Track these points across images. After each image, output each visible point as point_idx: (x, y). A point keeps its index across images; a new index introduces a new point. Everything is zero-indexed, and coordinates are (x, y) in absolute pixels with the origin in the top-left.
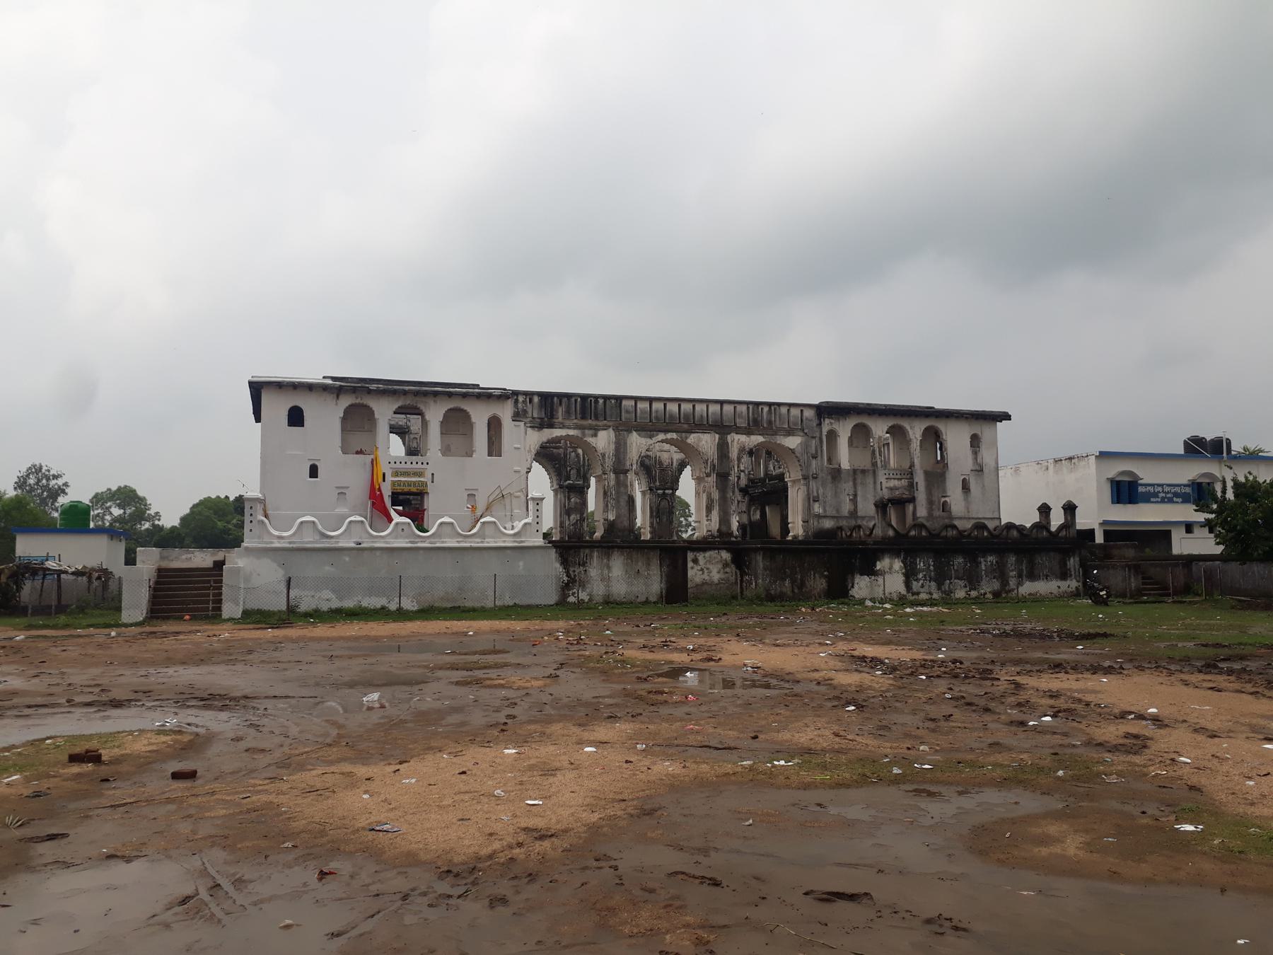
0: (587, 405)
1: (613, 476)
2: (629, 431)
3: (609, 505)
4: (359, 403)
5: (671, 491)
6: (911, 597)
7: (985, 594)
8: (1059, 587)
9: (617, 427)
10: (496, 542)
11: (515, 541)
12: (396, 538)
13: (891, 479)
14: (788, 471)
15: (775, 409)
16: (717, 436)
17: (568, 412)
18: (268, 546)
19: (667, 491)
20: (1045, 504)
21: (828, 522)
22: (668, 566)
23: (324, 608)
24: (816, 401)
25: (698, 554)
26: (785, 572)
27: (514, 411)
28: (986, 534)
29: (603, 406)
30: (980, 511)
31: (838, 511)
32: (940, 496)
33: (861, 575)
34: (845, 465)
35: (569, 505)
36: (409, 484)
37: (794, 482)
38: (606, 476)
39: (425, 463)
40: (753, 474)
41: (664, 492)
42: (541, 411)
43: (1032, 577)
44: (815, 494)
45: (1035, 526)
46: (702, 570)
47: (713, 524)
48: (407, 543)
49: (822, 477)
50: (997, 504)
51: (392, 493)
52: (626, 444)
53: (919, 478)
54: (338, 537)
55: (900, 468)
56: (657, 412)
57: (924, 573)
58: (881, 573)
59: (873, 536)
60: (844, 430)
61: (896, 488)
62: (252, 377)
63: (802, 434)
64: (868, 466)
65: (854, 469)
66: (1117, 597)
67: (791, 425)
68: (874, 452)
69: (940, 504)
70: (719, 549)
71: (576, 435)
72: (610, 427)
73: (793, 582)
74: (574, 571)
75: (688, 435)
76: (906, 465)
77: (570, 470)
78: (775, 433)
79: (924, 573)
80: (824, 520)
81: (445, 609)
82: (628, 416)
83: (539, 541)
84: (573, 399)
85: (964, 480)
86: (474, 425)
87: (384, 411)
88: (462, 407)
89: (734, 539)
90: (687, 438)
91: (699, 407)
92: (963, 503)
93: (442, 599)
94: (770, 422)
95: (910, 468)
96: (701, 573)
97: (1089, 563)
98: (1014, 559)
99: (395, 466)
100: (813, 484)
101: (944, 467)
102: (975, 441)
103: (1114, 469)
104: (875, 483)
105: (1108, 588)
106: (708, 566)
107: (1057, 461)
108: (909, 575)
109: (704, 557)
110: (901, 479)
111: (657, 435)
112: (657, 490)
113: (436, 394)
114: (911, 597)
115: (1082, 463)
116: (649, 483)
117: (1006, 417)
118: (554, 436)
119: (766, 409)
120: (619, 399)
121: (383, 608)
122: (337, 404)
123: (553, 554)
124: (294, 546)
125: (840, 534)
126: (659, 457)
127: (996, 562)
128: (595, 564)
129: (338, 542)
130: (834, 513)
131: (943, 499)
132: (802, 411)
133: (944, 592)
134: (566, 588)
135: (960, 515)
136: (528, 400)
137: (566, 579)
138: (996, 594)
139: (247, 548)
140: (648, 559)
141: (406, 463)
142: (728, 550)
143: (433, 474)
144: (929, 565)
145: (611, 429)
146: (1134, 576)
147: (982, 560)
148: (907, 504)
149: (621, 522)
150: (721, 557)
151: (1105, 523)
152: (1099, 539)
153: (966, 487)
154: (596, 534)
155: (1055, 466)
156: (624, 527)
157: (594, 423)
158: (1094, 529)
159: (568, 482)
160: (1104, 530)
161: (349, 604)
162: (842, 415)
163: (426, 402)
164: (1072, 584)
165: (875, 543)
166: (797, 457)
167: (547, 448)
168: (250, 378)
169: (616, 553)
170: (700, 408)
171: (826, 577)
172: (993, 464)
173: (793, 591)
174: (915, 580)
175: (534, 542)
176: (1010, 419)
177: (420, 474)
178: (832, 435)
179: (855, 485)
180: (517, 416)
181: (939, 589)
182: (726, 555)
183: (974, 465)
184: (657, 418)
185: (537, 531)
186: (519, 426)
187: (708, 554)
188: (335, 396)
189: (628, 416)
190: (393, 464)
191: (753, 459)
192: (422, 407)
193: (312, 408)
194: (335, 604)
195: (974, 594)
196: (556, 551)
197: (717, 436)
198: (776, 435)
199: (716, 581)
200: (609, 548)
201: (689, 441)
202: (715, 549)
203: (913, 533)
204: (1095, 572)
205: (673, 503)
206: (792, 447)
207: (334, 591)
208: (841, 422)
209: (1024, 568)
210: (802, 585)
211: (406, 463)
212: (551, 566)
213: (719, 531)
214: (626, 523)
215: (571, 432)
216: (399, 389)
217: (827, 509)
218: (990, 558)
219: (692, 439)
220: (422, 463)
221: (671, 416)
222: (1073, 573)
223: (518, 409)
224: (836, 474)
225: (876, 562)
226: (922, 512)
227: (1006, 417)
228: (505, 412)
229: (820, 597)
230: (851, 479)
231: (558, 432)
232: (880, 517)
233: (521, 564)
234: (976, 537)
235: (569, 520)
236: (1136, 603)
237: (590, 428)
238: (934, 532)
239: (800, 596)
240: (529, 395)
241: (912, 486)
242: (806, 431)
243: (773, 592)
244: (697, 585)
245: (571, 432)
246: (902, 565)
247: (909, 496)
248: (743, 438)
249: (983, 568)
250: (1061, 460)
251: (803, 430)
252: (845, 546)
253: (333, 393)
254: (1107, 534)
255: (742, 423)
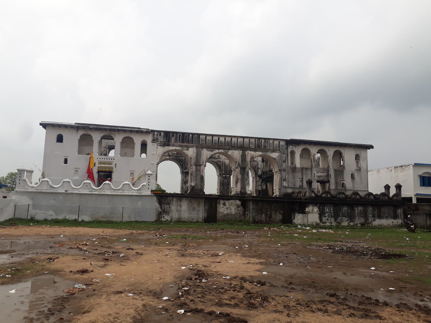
0: (184, 137)
1: (194, 167)
2: (203, 148)
3: (192, 179)
4: (87, 134)
5: (229, 176)
6: (322, 224)
7: (357, 224)
8: (393, 222)
9: (197, 146)
10: (129, 193)
11: (137, 193)
12: (84, 189)
13: (319, 172)
14: (274, 168)
15: (267, 141)
16: (241, 152)
17: (176, 140)
18: (26, 190)
19: (227, 176)
20: (388, 184)
21: (289, 190)
22: (208, 206)
23: (49, 218)
24: (288, 138)
25: (226, 201)
26: (263, 211)
27: (153, 139)
28: (358, 197)
29: (191, 138)
30: (359, 187)
31: (294, 185)
32: (341, 180)
33: (299, 213)
34: (298, 165)
35: (185, 180)
36: (105, 168)
37: (276, 172)
38: (192, 167)
39: (113, 159)
40: (264, 170)
41: (226, 176)
42: (164, 139)
43: (380, 217)
44: (284, 178)
45: (382, 194)
46: (227, 208)
47: (238, 189)
48: (88, 192)
49: (288, 170)
50: (367, 185)
51: (98, 171)
52: (201, 154)
53: (332, 172)
54: (58, 188)
55: (324, 168)
56: (215, 141)
57: (328, 214)
58: (309, 213)
59: (306, 196)
60: (298, 150)
61: (321, 176)
62: (42, 122)
63: (279, 152)
64: (310, 167)
65: (302, 168)
66: (420, 228)
67: (274, 147)
68: (311, 160)
69: (341, 184)
70: (235, 199)
71: (179, 149)
72: (194, 146)
73: (266, 215)
74: (164, 207)
75: (228, 151)
76: (326, 167)
77: (187, 166)
78: (267, 151)
79: (328, 214)
80: (288, 189)
81: (104, 222)
82: (202, 142)
83: (149, 193)
84: (178, 135)
85: (352, 174)
86: (94, 141)
87: (96, 137)
88: (130, 136)
89: (247, 196)
90: (228, 152)
91: (233, 139)
92: (351, 184)
93: (103, 217)
94: (265, 146)
95: (328, 168)
96: (227, 209)
97: (407, 212)
98: (371, 209)
99: (100, 160)
100: (283, 173)
101: (343, 168)
102: (357, 157)
103: (422, 171)
104: (311, 174)
105: (415, 224)
106: (230, 206)
107: (395, 168)
108: (321, 214)
109: (228, 203)
110: (323, 172)
111: (215, 150)
112: (223, 175)
113: (119, 130)
114: (322, 224)
115: (407, 168)
116: (220, 172)
117: (371, 147)
118: (170, 149)
119: (263, 141)
120: (199, 135)
121: (75, 220)
122: (77, 134)
123: (155, 198)
124: (37, 191)
125: (293, 195)
126: (224, 161)
127: (363, 210)
128: (174, 204)
129: (57, 190)
130: (293, 186)
131: (342, 182)
132: (279, 142)
133: (338, 223)
134: (160, 215)
135: (350, 189)
136: (159, 134)
137: (160, 210)
138: (362, 225)
139: (16, 191)
140: (199, 202)
141: (104, 159)
142: (239, 200)
143: (116, 164)
144: (331, 210)
145: (194, 147)
146: (429, 219)
147: (356, 209)
148: (326, 183)
149: (198, 187)
150: (236, 203)
151: (417, 194)
152: (414, 201)
153: (353, 176)
154: (232, 193)
155: (395, 169)
156: (199, 188)
157: (188, 144)
158: (412, 197)
159: (186, 170)
160: (416, 198)
161: (60, 217)
162: (297, 144)
163: (115, 134)
164: (399, 221)
165: (306, 199)
166: (276, 161)
167: (178, 156)
168: (41, 122)
169: (184, 199)
170: (234, 140)
171: (281, 214)
172: (365, 167)
173: (266, 219)
174: (324, 217)
175: (147, 193)
176: (373, 148)
177: (111, 164)
178: (293, 153)
179: (302, 174)
180: (154, 141)
181: (335, 221)
182: (238, 202)
183: (357, 167)
184: (215, 143)
185: (148, 188)
186: (154, 145)
187: (230, 201)
188: (76, 130)
189: (202, 142)
190: (99, 159)
191: (264, 163)
192: (113, 136)
193: (66, 135)
194: (54, 217)
195: (352, 224)
196: (156, 198)
197: (241, 152)
198: (267, 152)
199: (233, 213)
200: (181, 197)
201: (229, 153)
202: (233, 199)
203: (324, 195)
204: (409, 216)
205: (229, 180)
206: (274, 157)
207: (54, 212)
208: (297, 147)
209: (376, 213)
210: (271, 216)
211: (104, 159)
212: (154, 204)
213: (240, 192)
214: (199, 187)
215: (177, 148)
216: (102, 128)
217: (289, 184)
218: (360, 208)
219: (230, 152)
220: (112, 159)
221: (221, 143)
222: (400, 216)
223: (154, 138)
224: (294, 169)
225: (306, 208)
226: (333, 187)
227: (371, 147)
228: (149, 139)
229: (279, 222)
230: (301, 172)
231: (171, 148)
232: (308, 188)
233: (140, 203)
234: (354, 198)
235: (185, 186)
236: (428, 232)
237: (186, 146)
238: (334, 196)
239: (269, 222)
240: (159, 132)
241: (328, 176)
242: (280, 151)
243: (256, 220)
244: (225, 215)
245: (177, 148)
246: (318, 210)
247: (327, 180)
248: (253, 153)
249: (357, 212)
250: (398, 167)
251: (280, 150)
252: (291, 200)
253: (76, 129)
254: (418, 199)
255: (252, 146)
